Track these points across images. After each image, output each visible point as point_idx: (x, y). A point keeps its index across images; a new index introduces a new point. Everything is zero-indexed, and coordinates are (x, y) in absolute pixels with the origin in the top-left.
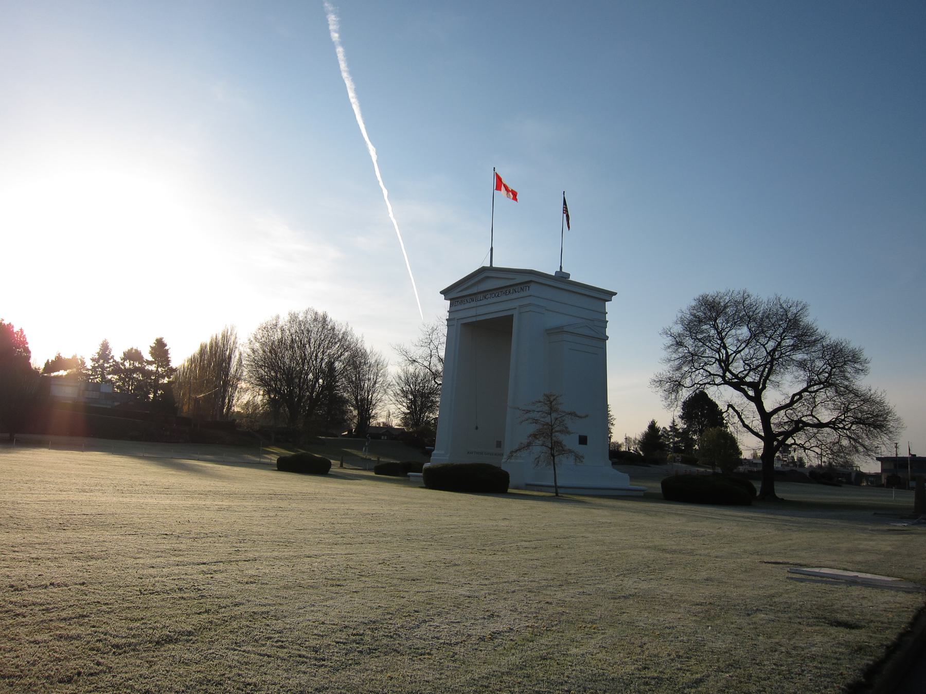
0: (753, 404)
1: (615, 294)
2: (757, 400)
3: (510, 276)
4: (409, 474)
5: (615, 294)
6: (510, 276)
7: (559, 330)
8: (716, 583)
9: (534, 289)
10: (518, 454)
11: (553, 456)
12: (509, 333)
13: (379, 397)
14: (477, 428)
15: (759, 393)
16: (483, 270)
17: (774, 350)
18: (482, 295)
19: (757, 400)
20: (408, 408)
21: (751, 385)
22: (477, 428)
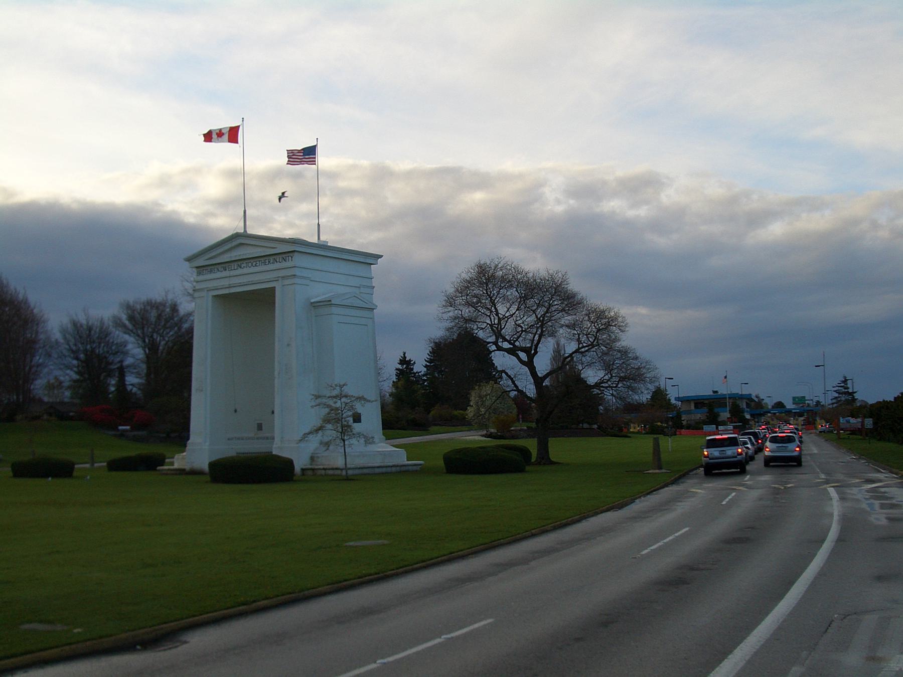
0: (526, 369)
1: (381, 256)
2: (530, 364)
3: (273, 245)
4: (158, 468)
5: (381, 256)
6: (273, 245)
7: (328, 303)
8: (362, 440)
9: (298, 260)
10: (311, 436)
11: (344, 441)
12: (273, 303)
13: (41, 361)
14: (236, 411)
15: (531, 357)
16: (236, 236)
17: (544, 316)
18: (236, 264)
19: (530, 364)
20: (78, 373)
21: (526, 350)
22: (236, 411)
